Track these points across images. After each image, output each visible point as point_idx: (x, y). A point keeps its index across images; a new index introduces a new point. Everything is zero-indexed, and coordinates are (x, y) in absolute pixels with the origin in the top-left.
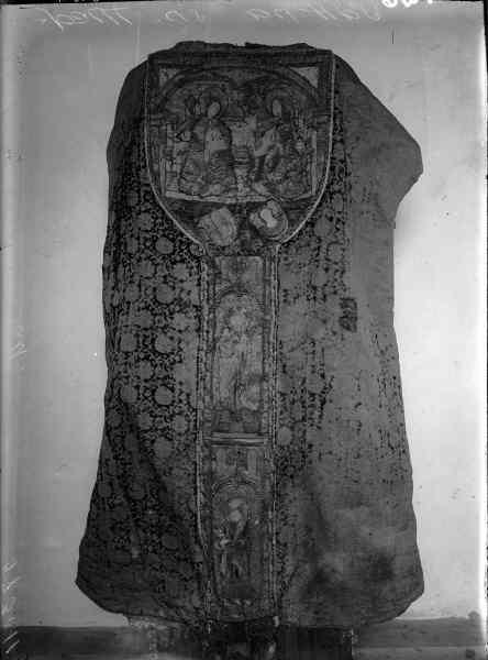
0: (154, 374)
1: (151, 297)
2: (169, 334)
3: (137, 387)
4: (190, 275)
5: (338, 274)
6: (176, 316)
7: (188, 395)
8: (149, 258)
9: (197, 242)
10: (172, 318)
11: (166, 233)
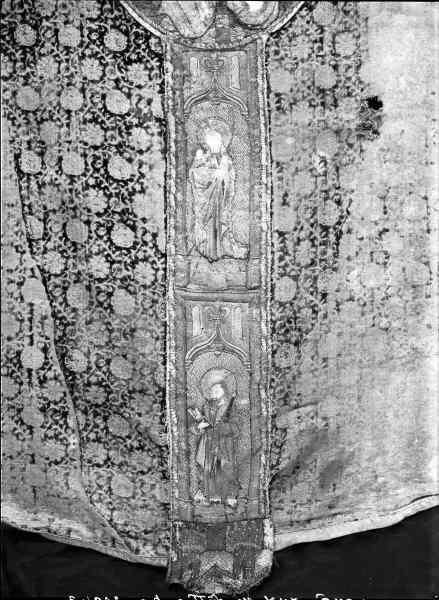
0: (109, 207)
1: (100, 106)
2: (126, 155)
3: (88, 223)
4: (150, 79)
5: (352, 70)
6: (135, 131)
7: (155, 236)
8: (94, 55)
9: (158, 34)
10: (129, 134)
11: (118, 23)
